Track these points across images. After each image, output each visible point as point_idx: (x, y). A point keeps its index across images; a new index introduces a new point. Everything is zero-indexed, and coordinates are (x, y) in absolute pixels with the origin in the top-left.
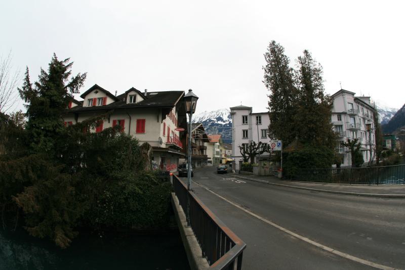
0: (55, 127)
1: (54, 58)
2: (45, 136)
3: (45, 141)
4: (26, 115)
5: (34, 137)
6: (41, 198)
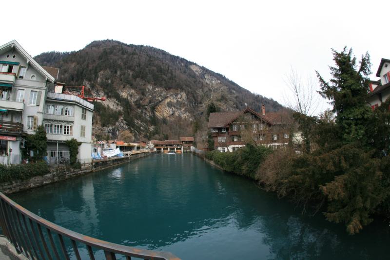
0: (363, 113)
1: (334, 53)
2: (356, 125)
3: (356, 130)
4: (334, 111)
5: (346, 128)
6: (349, 186)
